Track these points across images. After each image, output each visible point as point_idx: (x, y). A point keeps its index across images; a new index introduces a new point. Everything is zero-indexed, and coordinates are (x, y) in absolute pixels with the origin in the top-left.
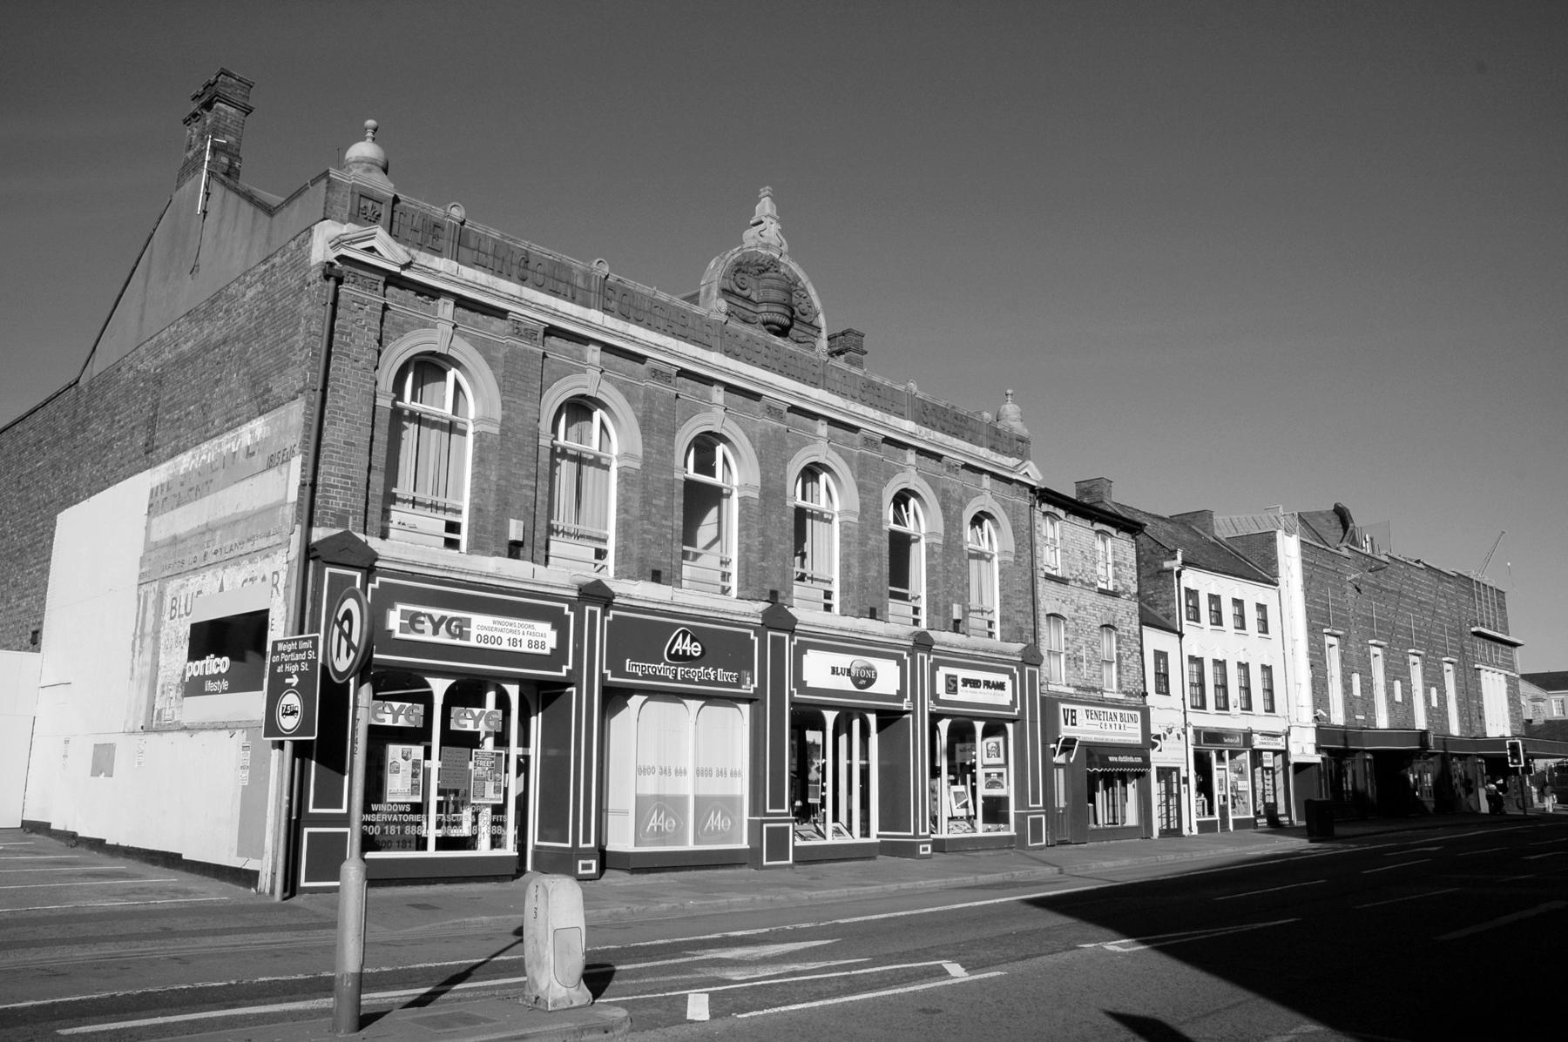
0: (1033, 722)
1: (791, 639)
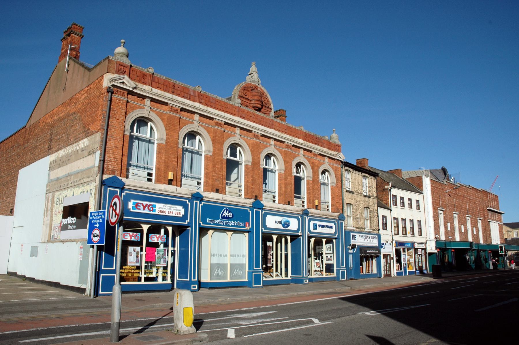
0: (342, 239)
1: (262, 212)
